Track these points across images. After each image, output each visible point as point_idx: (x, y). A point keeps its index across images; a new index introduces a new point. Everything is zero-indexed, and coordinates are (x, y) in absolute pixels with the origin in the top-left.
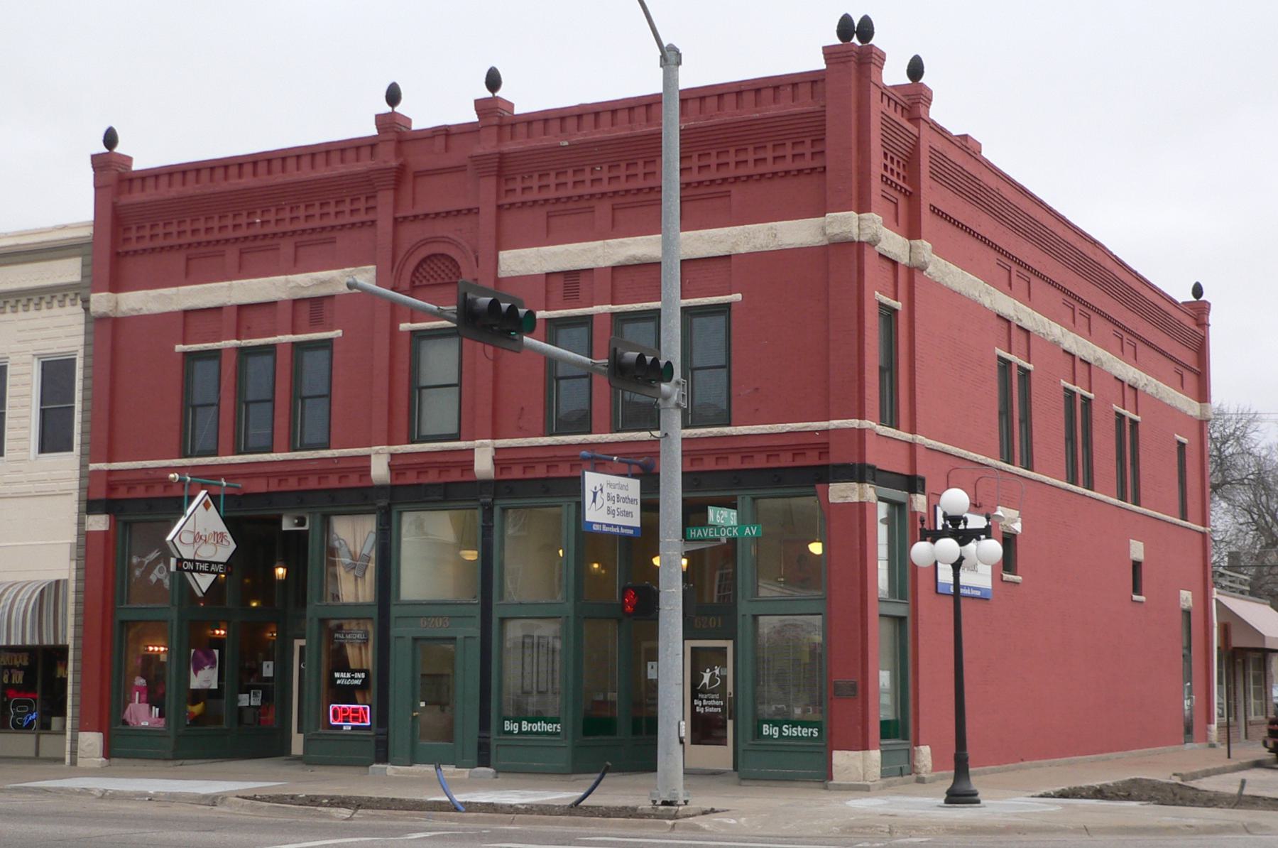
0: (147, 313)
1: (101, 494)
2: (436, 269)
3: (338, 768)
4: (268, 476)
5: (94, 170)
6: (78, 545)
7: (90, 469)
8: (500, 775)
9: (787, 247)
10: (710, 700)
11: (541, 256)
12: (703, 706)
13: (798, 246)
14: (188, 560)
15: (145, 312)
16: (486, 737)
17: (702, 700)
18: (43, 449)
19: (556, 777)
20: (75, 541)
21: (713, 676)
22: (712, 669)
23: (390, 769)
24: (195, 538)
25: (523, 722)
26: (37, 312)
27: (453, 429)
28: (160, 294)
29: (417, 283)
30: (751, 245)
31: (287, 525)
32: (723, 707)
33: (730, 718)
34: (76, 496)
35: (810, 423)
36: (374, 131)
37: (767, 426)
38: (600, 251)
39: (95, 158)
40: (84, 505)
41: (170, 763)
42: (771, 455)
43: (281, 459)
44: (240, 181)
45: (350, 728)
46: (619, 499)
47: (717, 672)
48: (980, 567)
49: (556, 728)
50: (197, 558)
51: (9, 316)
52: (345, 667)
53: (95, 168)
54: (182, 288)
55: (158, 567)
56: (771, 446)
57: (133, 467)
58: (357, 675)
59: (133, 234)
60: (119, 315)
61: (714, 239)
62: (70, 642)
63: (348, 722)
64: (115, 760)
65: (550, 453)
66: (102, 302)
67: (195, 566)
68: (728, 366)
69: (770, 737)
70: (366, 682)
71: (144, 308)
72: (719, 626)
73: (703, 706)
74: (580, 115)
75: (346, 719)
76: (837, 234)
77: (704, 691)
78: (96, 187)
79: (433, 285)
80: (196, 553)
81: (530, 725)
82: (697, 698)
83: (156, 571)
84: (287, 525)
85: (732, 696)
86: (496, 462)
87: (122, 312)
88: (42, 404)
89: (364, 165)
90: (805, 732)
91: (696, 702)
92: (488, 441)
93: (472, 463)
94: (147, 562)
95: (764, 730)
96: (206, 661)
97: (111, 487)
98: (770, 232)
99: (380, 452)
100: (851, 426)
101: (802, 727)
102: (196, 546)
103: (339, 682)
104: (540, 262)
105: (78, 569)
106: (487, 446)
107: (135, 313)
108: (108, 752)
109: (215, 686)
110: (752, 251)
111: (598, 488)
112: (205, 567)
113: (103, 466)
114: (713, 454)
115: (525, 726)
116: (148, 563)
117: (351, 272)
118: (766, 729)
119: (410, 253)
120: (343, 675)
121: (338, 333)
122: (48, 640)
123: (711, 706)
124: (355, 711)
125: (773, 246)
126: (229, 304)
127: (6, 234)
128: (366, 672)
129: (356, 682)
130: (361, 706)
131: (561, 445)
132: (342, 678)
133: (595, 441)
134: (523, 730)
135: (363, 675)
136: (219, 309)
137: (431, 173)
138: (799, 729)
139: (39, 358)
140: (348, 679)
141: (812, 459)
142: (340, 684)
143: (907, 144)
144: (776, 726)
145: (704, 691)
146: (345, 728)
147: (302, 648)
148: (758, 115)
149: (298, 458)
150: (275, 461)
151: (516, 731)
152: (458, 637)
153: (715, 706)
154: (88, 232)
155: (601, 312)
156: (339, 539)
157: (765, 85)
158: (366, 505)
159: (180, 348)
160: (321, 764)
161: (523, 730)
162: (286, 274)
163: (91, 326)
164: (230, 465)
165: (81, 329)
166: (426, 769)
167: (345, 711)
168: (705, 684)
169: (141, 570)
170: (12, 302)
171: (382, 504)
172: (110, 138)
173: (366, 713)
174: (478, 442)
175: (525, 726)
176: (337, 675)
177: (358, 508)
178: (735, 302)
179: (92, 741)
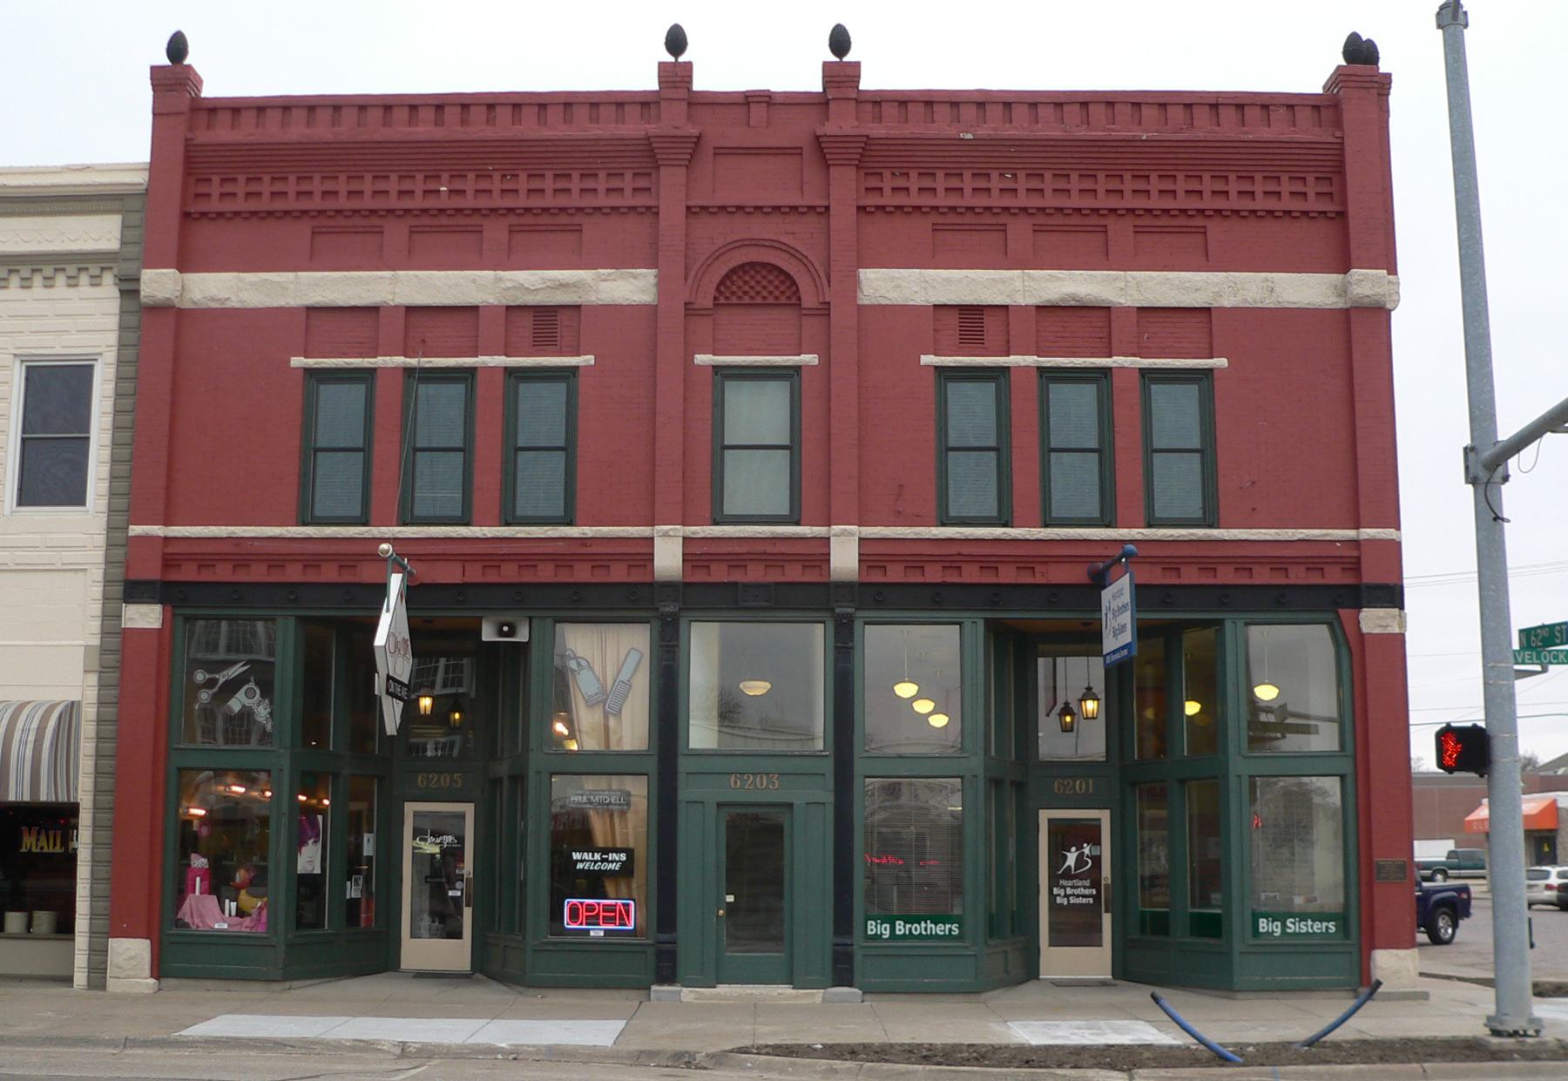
0: (237, 305)
1: (153, 572)
4: (465, 559)
5: (154, 90)
6: (104, 650)
7: (131, 533)
8: (868, 997)
9: (1288, 306)
10: (1077, 887)
11: (926, 281)
12: (1066, 896)
13: (1303, 306)
15: (234, 303)
16: (847, 945)
17: (1064, 888)
18: (22, 501)
19: (958, 997)
20: (96, 641)
21: (1081, 855)
22: (1080, 848)
23: (687, 994)
25: (897, 922)
26: (71, 292)
27: (784, 509)
28: (265, 280)
29: (722, 301)
30: (1239, 298)
31: (488, 634)
32: (1097, 898)
34: (97, 573)
35: (1330, 531)
36: (653, 85)
37: (258, 528)
38: (1018, 284)
39: (156, 71)
41: (276, 987)
42: (238, 565)
43: (489, 536)
44: (411, 129)
45: (602, 934)
47: (1086, 851)
48: (1322, 725)
51: (14, 291)
52: (587, 843)
53: (155, 86)
54: (304, 275)
55: (246, 687)
56: (1278, 555)
59: (215, 188)
60: (187, 305)
61: (1187, 285)
62: (85, 798)
63: (599, 924)
64: (172, 982)
65: (953, 550)
66: (159, 283)
68: (945, 449)
69: (1270, 934)
71: (234, 299)
72: (1091, 790)
73: (1066, 896)
75: (594, 920)
76: (1368, 296)
77: (1068, 875)
78: (155, 114)
79: (759, 305)
81: (908, 926)
82: (1057, 885)
83: (241, 694)
84: (488, 634)
85: (1109, 882)
86: (687, 558)
87: (194, 302)
88: (24, 432)
89: (633, 128)
90: (1318, 927)
91: (1056, 891)
92: (854, 528)
93: (650, 557)
94: (222, 680)
95: (1261, 925)
96: (310, 833)
97: (169, 562)
98: (1265, 285)
99: (671, 533)
100: (1391, 537)
101: (1313, 921)
103: (580, 866)
104: (925, 288)
105: (102, 686)
106: (851, 534)
108: (160, 969)
109: (318, 871)
110: (1241, 305)
113: (158, 530)
114: (977, 561)
115: (901, 929)
117: (610, 274)
118: (1264, 925)
119: (717, 256)
120: (586, 856)
121: (587, 360)
122: (63, 798)
123: (1078, 896)
124: (607, 908)
125: (1269, 303)
126: (392, 303)
128: (630, 852)
129: (611, 866)
132: (584, 860)
133: (1020, 537)
134: (898, 932)
135: (623, 857)
136: (373, 310)
138: (1310, 923)
139: (22, 361)
140: (596, 862)
141: (1334, 576)
143: (201, 160)
145: (1068, 875)
146: (592, 933)
149: (519, 536)
151: (887, 934)
152: (796, 802)
153: (1084, 896)
154: (142, 178)
155: (1022, 364)
156: (576, 658)
159: (297, 361)
160: (597, 988)
161: (898, 932)
162: (494, 268)
163: (133, 320)
164: (967, 540)
165: (113, 322)
166: (749, 991)
167: (590, 908)
168: (1069, 867)
169: (211, 692)
170: (25, 272)
171: (667, 609)
172: (177, 48)
174: (836, 529)
175: (901, 929)
177: (622, 614)
178: (1219, 369)
179: (131, 953)
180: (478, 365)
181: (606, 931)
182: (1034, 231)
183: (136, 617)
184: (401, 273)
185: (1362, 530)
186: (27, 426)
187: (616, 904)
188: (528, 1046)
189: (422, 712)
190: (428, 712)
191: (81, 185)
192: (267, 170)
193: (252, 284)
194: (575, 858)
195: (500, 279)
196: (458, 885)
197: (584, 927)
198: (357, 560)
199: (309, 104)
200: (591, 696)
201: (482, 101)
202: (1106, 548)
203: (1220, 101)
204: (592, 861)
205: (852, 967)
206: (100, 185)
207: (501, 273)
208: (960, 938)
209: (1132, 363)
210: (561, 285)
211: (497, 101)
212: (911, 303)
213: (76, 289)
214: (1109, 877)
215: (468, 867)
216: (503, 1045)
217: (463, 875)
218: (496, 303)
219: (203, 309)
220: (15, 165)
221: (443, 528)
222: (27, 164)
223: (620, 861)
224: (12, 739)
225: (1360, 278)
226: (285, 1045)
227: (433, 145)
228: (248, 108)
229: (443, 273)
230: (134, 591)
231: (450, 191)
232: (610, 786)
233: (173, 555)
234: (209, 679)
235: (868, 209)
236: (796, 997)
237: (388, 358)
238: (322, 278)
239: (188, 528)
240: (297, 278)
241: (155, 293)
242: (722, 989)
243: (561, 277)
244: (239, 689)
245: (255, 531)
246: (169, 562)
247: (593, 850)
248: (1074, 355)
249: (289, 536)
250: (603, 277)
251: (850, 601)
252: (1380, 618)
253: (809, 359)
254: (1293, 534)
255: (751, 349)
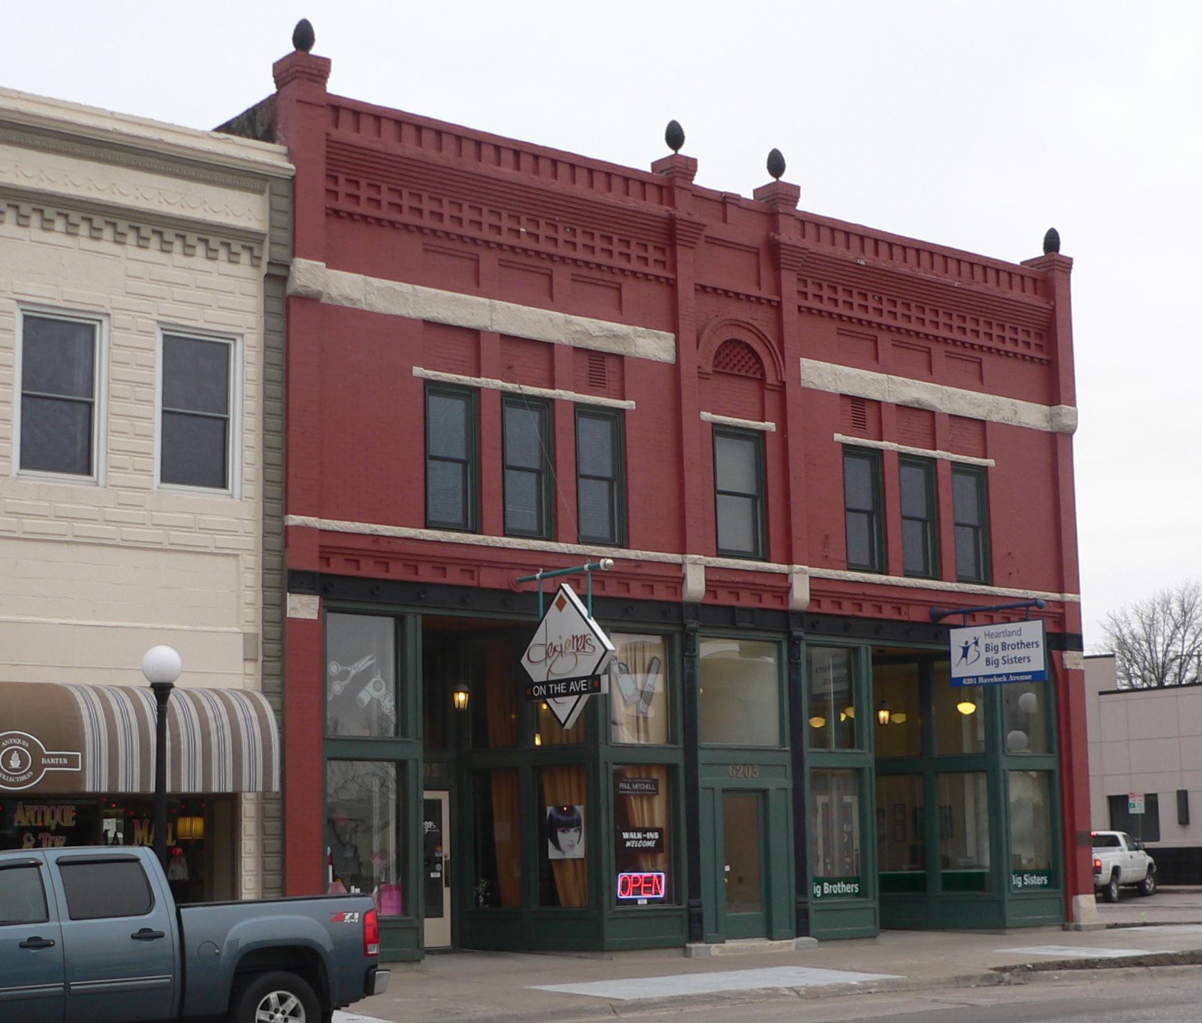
0: (367, 308)
1: (312, 564)
2: (728, 360)
3: (644, 953)
14: (539, 684)
19: (865, 941)
23: (715, 949)
24: (547, 653)
27: (747, 546)
28: (390, 288)
30: (1001, 416)
33: (447, 886)
40: (275, 579)
45: (645, 902)
46: (1014, 646)
49: (854, 889)
50: (551, 678)
51: (10, 227)
55: (374, 680)
57: (357, 531)
58: (650, 835)
61: (975, 401)
63: (640, 894)
67: (548, 689)
68: (427, 457)
70: (659, 842)
74: (520, 152)
75: (637, 891)
76: (1069, 426)
80: (549, 670)
81: (831, 886)
83: (370, 687)
85: (449, 858)
94: (353, 673)
97: (325, 555)
99: (698, 562)
102: (549, 661)
103: (628, 844)
106: (805, 572)
107: (347, 304)
110: (1001, 421)
111: (971, 641)
112: (561, 688)
116: (355, 676)
117: (643, 331)
120: (633, 835)
124: (648, 881)
127: (112, 113)
128: (659, 830)
129: (649, 844)
130: (655, 874)
131: (866, 583)
134: (825, 892)
135: (656, 835)
137: (738, 247)
140: (639, 840)
142: (630, 847)
144: (819, 884)
146: (639, 902)
147: (826, 805)
148: (884, 265)
150: (565, 554)
157: (651, 181)
158: (667, 624)
159: (418, 371)
161: (825, 892)
164: (882, 585)
166: (752, 944)
167: (636, 880)
172: (303, 35)
173: (660, 882)
174: (797, 567)
176: (626, 835)
180: (556, 397)
181: (649, 900)
182: (500, 265)
183: (299, 606)
184: (497, 302)
185: (1066, 594)
186: (25, 384)
187: (652, 877)
188: (872, 982)
189: (882, 722)
190: (887, 722)
191: (236, 158)
192: (386, 179)
193: (378, 289)
194: (625, 837)
195: (570, 322)
196: (438, 867)
197: (631, 897)
198: (762, 590)
199: (816, 221)
200: (630, 697)
201: (452, 131)
202: (938, 596)
203: (989, 265)
204: (636, 840)
205: (808, 921)
206: (255, 162)
207: (573, 317)
208: (858, 895)
209: (756, 425)
210: (614, 336)
211: (560, 159)
212: (828, 390)
213: (27, 229)
214: (859, 848)
215: (446, 849)
216: (855, 983)
217: (441, 858)
218: (567, 343)
219: (362, 311)
220: (156, 118)
221: (540, 542)
222: (37, 92)
223: (654, 839)
224: (239, 731)
225: (1067, 412)
226: (725, 998)
227: (584, 203)
228: (368, 114)
229: (526, 308)
230: (297, 581)
231: (528, 233)
232: (640, 775)
233: (330, 545)
234: (342, 671)
235: (626, 273)
236: (780, 947)
237: (489, 380)
238: (437, 294)
239: (336, 522)
240: (491, 306)
241: (310, 285)
242: (730, 944)
243: (615, 329)
244: (368, 682)
245: (393, 530)
246: (325, 555)
247: (636, 830)
248: (450, 371)
249: (422, 538)
250: (639, 333)
251: (694, 619)
252: (1075, 658)
253: (770, 426)
254: (1032, 594)
255: (451, 369)
